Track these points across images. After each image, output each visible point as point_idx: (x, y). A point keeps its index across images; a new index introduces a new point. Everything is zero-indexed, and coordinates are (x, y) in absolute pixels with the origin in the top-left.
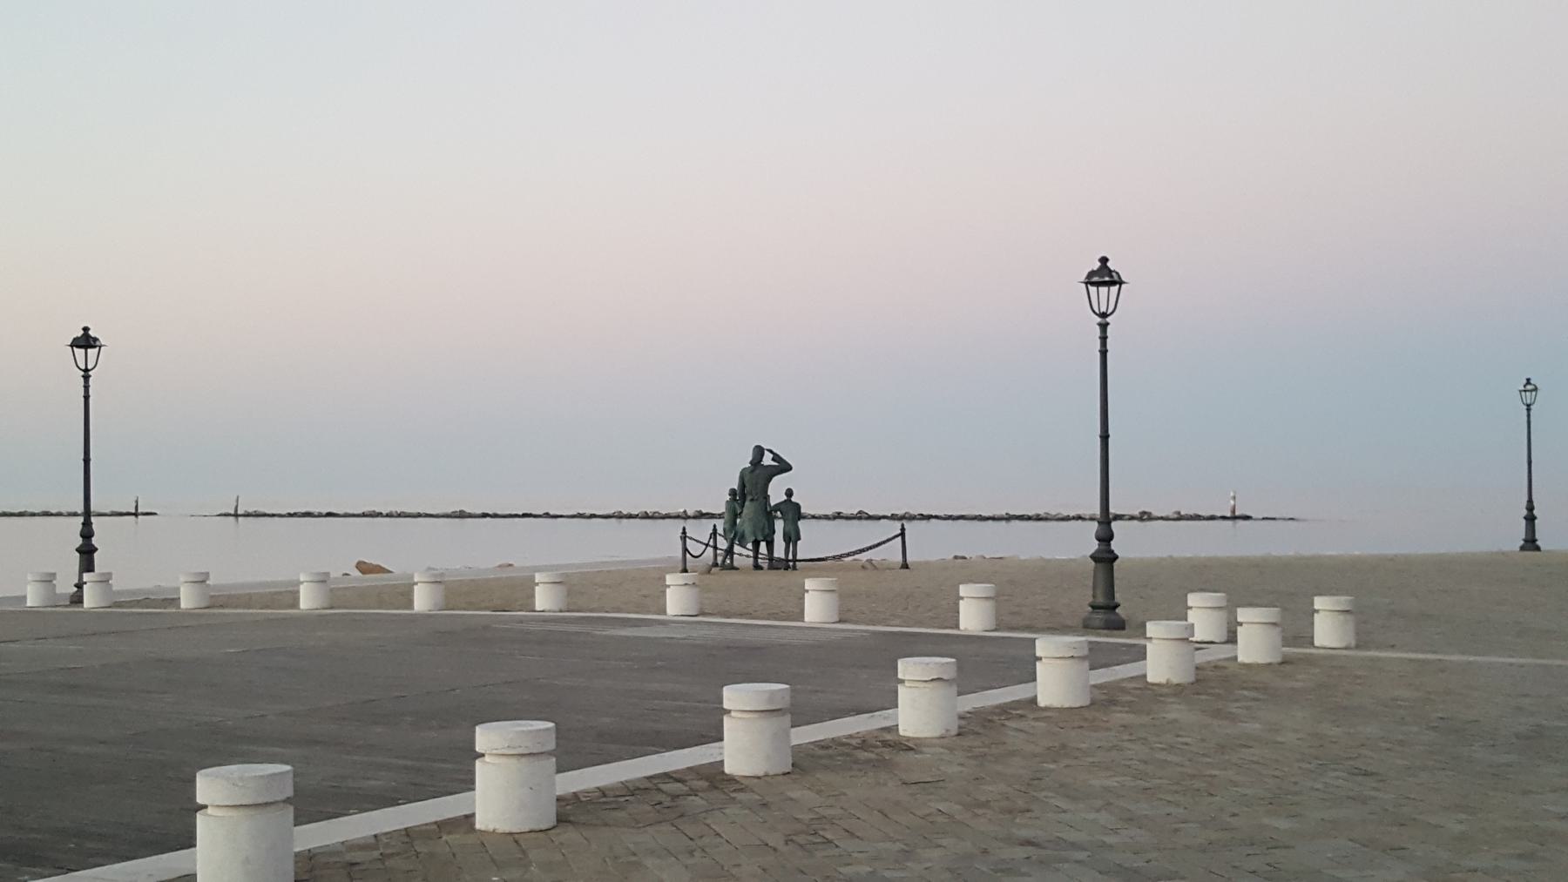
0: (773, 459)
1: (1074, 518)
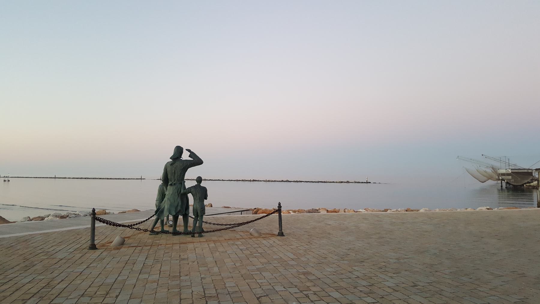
1: (332, 182)
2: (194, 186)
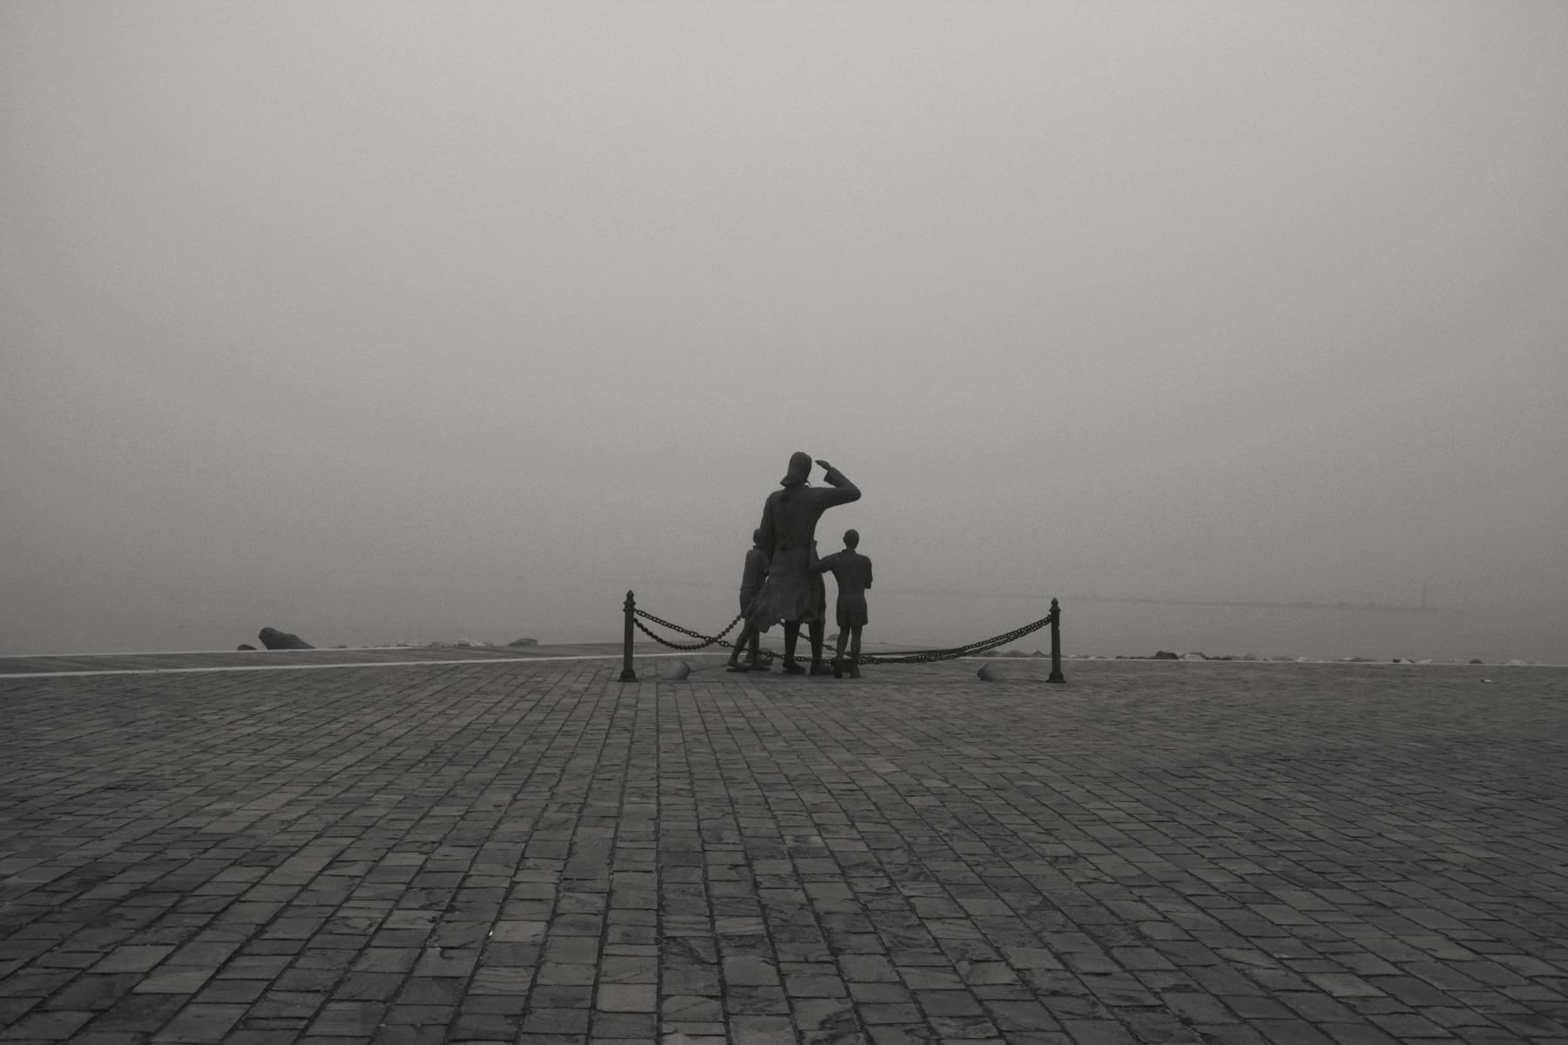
0: (827, 479)
2: (838, 553)
